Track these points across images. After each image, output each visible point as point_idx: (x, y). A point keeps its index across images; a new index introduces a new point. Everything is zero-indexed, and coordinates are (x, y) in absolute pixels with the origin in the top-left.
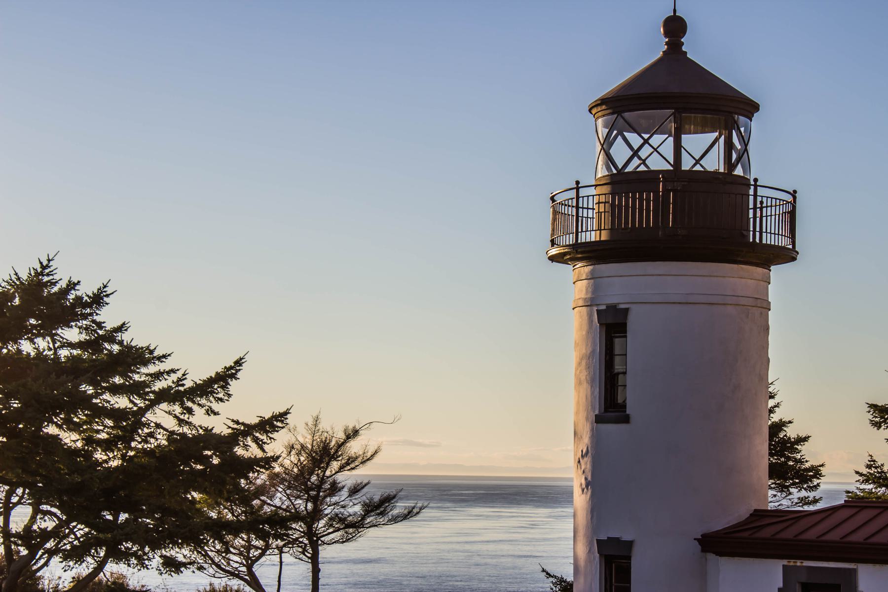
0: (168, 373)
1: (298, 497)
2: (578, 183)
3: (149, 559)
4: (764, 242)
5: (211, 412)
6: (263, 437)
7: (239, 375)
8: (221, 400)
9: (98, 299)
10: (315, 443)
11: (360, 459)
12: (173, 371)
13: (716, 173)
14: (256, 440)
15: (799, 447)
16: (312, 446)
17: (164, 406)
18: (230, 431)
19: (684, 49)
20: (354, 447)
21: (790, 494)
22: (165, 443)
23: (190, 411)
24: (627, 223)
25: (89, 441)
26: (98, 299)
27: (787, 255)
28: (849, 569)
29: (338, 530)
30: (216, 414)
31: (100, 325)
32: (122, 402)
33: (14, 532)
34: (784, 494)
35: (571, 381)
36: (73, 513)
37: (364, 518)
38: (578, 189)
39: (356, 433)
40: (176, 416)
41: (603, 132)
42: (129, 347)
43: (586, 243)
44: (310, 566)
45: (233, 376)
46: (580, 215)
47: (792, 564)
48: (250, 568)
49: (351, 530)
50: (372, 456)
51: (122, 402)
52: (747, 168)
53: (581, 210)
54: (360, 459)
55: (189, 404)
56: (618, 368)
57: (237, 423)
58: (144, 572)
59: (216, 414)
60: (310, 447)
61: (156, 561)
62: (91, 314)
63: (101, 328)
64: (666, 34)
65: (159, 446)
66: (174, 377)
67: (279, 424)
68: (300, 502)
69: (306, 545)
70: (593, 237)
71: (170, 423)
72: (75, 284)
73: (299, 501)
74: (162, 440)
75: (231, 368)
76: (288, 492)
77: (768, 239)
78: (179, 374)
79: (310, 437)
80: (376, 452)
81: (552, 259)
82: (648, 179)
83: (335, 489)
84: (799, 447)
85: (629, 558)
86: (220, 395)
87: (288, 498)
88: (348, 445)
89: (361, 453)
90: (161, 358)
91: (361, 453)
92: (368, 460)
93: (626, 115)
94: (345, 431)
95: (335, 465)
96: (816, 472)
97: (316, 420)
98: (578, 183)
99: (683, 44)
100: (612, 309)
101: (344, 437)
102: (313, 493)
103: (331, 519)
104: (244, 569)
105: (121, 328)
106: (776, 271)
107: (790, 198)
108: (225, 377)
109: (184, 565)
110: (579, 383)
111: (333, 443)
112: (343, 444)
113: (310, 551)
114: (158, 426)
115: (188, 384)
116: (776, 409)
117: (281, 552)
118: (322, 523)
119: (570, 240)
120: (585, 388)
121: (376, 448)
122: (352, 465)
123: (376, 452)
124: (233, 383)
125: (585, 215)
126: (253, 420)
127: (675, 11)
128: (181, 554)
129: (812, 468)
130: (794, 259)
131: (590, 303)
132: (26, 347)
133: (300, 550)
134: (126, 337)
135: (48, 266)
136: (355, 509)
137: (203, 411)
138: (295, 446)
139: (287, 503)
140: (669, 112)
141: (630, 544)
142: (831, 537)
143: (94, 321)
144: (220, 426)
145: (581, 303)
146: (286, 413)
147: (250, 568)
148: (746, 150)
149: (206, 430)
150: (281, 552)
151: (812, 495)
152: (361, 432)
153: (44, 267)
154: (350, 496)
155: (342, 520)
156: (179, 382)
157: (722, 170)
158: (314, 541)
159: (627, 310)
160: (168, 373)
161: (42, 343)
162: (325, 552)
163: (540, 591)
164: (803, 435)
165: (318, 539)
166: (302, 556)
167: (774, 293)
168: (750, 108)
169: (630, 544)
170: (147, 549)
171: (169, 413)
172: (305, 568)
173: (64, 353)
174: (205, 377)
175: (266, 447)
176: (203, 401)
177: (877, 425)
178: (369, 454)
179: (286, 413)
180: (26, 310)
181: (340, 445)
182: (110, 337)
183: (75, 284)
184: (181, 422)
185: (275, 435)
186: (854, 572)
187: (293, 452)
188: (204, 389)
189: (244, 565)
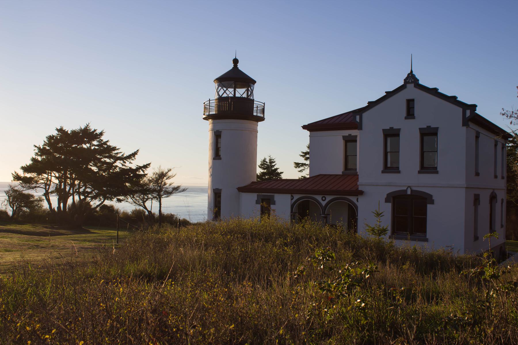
0: (120, 153)
2: (210, 99)
3: (113, 199)
5: (130, 163)
6: (144, 170)
7: (138, 154)
8: (133, 160)
9: (101, 134)
12: (121, 152)
13: (245, 97)
14: (142, 170)
17: (119, 161)
18: (136, 168)
19: (238, 67)
22: (119, 170)
23: (125, 162)
24: (223, 109)
26: (101, 134)
27: (262, 119)
31: (102, 140)
32: (108, 160)
33: (131, 213)
35: (208, 149)
36: (94, 188)
37: (172, 191)
38: (209, 101)
39: (170, 170)
40: (121, 164)
41: (217, 87)
42: (110, 146)
44: (159, 203)
45: (136, 154)
51: (108, 160)
55: (125, 161)
56: (219, 146)
57: (138, 166)
58: (112, 202)
61: (115, 199)
62: (100, 138)
63: (102, 141)
64: (233, 63)
65: (117, 171)
66: (121, 154)
67: (148, 166)
70: (214, 113)
71: (120, 166)
72: (96, 130)
74: (118, 170)
75: (136, 152)
77: (259, 115)
78: (123, 153)
80: (175, 175)
81: (204, 119)
82: (227, 98)
85: (221, 193)
86: (133, 159)
90: (118, 149)
93: (222, 83)
94: (168, 169)
95: (165, 178)
97: (160, 166)
98: (210, 99)
102: (160, 185)
103: (165, 192)
105: (107, 141)
106: (260, 123)
108: (134, 154)
109: (122, 200)
110: (210, 150)
112: (167, 173)
113: (159, 199)
115: (125, 156)
117: (152, 200)
118: (162, 193)
119: (208, 114)
120: (211, 151)
123: (175, 175)
124: (136, 156)
126: (142, 165)
128: (121, 198)
130: (264, 120)
131: (213, 130)
132: (84, 146)
134: (108, 144)
135: (88, 125)
137: (128, 162)
140: (233, 82)
141: (221, 190)
142: (269, 187)
143: (100, 139)
144: (134, 167)
145: (210, 130)
146: (150, 164)
148: (252, 92)
149: (130, 167)
150: (152, 200)
153: (87, 125)
155: (167, 192)
156: (123, 155)
157: (246, 97)
159: (221, 132)
160: (120, 153)
161: (88, 145)
162: (162, 200)
163: (107, 161)
164: (282, 172)
168: (254, 82)
169: (221, 190)
170: (113, 196)
171: (120, 163)
172: (158, 204)
173: (93, 148)
174: (129, 154)
175: (145, 172)
176: (128, 160)
177: (296, 167)
179: (150, 164)
180: (84, 136)
181: (167, 173)
182: (105, 143)
183: (96, 130)
184: (123, 165)
185: (147, 169)
186: (273, 196)
188: (130, 157)
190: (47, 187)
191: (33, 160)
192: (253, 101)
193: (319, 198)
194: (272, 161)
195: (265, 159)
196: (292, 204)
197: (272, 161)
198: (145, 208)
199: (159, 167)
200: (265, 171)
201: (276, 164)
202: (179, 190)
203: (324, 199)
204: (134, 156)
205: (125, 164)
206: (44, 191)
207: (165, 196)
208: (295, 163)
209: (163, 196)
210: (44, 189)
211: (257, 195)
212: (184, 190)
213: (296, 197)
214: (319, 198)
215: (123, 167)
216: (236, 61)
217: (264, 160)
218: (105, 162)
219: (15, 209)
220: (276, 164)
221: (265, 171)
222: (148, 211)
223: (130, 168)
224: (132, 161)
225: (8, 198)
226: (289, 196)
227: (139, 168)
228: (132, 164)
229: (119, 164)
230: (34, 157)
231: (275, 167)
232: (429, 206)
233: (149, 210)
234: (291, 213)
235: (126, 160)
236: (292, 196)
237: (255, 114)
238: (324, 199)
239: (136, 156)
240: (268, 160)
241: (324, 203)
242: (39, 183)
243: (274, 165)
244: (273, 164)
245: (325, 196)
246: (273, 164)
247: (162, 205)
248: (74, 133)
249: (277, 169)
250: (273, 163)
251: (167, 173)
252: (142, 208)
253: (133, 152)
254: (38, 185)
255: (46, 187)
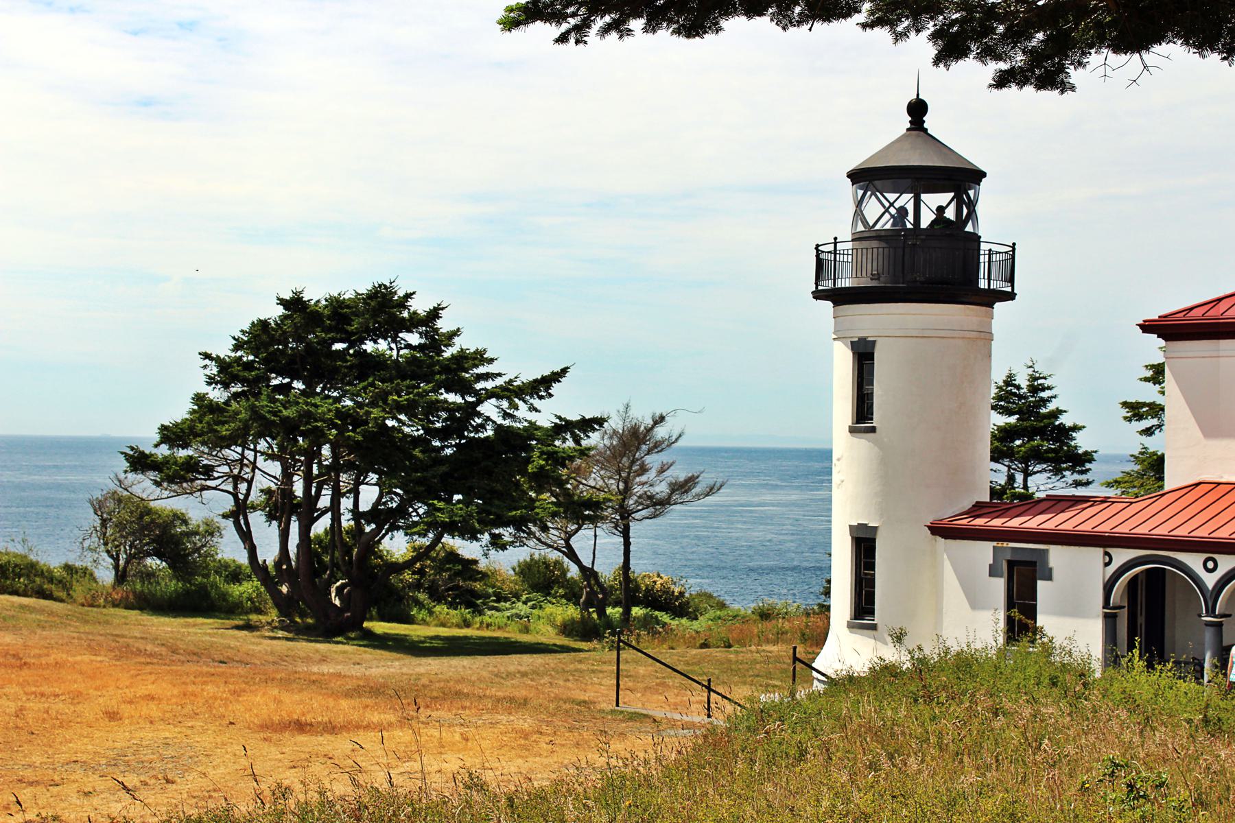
1: (610, 478)
2: (836, 239)
4: (992, 287)
5: (533, 409)
10: (625, 428)
11: (666, 443)
12: (500, 375)
15: (1074, 434)
16: (623, 430)
17: (493, 401)
19: (924, 119)
20: (661, 432)
21: (1064, 477)
25: (428, 431)
28: (1040, 550)
29: (648, 507)
30: (537, 410)
34: (1058, 477)
38: (835, 243)
39: (662, 418)
43: (842, 288)
44: (622, 540)
46: (838, 259)
47: (1000, 545)
48: (567, 541)
49: (658, 507)
50: (677, 440)
52: (975, 225)
53: (838, 256)
54: (666, 443)
59: (537, 410)
60: (621, 431)
68: (613, 481)
69: (617, 520)
73: (612, 481)
76: (602, 472)
77: (995, 285)
79: (621, 423)
80: (680, 436)
83: (643, 470)
84: (1074, 434)
86: (543, 393)
87: (602, 479)
88: (655, 429)
89: (667, 437)
90: (491, 361)
91: (667, 437)
92: (673, 443)
96: (1088, 457)
97: (627, 407)
98: (836, 239)
99: (924, 122)
100: (863, 341)
101: (652, 423)
104: (562, 542)
107: (1011, 249)
111: (642, 428)
114: (488, 419)
116: (1053, 399)
121: (680, 431)
122: (659, 449)
123: (680, 436)
125: (841, 260)
126: (574, 417)
127: (918, 95)
129: (1086, 453)
130: (1013, 299)
133: (613, 525)
136: (661, 489)
138: (608, 432)
139: (601, 483)
147: (567, 541)
151: (1083, 478)
152: (666, 418)
154: (658, 476)
155: (651, 497)
158: (625, 514)
159: (874, 342)
162: (633, 526)
165: (630, 515)
166: (614, 531)
167: (996, 328)
178: (673, 439)
181: (649, 430)
184: (506, 415)
187: (606, 437)
188: (541, 386)
189: (562, 539)
190: (243, 487)
191: (199, 399)
192: (975, 239)
193: (1194, 561)
194: (1040, 381)
195: (1010, 376)
196: (1107, 579)
197: (1040, 381)
198: (572, 555)
199: (622, 409)
200: (1013, 419)
201: (1055, 397)
202: (694, 491)
203: (1210, 565)
204: (548, 388)
205: (516, 413)
206: (228, 503)
207: (644, 513)
208: (1125, 404)
209: (637, 516)
210: (231, 497)
211: (994, 547)
212: (711, 489)
213: (1121, 556)
214: (1194, 561)
215: (507, 422)
216: (917, 109)
217: (1009, 381)
218: (445, 406)
219: (122, 562)
220: (1055, 397)
221: (1013, 419)
222: (582, 568)
223: (532, 424)
224: (536, 402)
225: (99, 522)
226: (1095, 555)
227: (563, 427)
228: (544, 413)
229: (489, 408)
230: (204, 389)
231: (1051, 406)
232: (1041, 585)
233: (587, 562)
234: (1104, 608)
235: (556, 424)
236: (1106, 554)
237: (983, 284)
238: (1210, 565)
239: (556, 388)
240: (1022, 381)
241: (1210, 580)
242: (216, 475)
243: (1049, 399)
244: (1045, 394)
245: (1215, 556)
246: (1045, 394)
247: (632, 548)
248: (337, 305)
249: (1057, 413)
250: (1043, 390)
251: (649, 430)
252: (554, 555)
253: (547, 373)
254: (210, 483)
255: (235, 487)
